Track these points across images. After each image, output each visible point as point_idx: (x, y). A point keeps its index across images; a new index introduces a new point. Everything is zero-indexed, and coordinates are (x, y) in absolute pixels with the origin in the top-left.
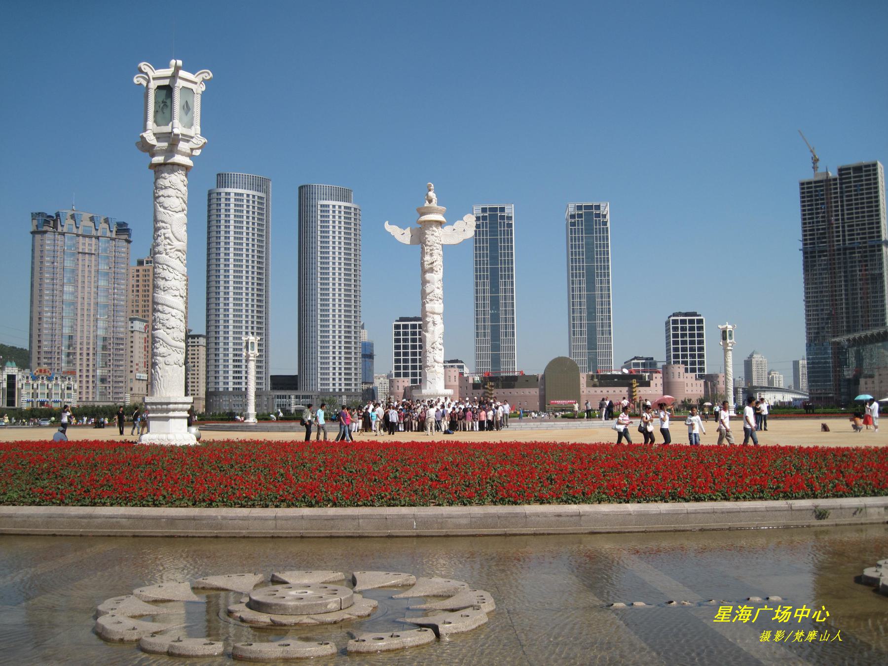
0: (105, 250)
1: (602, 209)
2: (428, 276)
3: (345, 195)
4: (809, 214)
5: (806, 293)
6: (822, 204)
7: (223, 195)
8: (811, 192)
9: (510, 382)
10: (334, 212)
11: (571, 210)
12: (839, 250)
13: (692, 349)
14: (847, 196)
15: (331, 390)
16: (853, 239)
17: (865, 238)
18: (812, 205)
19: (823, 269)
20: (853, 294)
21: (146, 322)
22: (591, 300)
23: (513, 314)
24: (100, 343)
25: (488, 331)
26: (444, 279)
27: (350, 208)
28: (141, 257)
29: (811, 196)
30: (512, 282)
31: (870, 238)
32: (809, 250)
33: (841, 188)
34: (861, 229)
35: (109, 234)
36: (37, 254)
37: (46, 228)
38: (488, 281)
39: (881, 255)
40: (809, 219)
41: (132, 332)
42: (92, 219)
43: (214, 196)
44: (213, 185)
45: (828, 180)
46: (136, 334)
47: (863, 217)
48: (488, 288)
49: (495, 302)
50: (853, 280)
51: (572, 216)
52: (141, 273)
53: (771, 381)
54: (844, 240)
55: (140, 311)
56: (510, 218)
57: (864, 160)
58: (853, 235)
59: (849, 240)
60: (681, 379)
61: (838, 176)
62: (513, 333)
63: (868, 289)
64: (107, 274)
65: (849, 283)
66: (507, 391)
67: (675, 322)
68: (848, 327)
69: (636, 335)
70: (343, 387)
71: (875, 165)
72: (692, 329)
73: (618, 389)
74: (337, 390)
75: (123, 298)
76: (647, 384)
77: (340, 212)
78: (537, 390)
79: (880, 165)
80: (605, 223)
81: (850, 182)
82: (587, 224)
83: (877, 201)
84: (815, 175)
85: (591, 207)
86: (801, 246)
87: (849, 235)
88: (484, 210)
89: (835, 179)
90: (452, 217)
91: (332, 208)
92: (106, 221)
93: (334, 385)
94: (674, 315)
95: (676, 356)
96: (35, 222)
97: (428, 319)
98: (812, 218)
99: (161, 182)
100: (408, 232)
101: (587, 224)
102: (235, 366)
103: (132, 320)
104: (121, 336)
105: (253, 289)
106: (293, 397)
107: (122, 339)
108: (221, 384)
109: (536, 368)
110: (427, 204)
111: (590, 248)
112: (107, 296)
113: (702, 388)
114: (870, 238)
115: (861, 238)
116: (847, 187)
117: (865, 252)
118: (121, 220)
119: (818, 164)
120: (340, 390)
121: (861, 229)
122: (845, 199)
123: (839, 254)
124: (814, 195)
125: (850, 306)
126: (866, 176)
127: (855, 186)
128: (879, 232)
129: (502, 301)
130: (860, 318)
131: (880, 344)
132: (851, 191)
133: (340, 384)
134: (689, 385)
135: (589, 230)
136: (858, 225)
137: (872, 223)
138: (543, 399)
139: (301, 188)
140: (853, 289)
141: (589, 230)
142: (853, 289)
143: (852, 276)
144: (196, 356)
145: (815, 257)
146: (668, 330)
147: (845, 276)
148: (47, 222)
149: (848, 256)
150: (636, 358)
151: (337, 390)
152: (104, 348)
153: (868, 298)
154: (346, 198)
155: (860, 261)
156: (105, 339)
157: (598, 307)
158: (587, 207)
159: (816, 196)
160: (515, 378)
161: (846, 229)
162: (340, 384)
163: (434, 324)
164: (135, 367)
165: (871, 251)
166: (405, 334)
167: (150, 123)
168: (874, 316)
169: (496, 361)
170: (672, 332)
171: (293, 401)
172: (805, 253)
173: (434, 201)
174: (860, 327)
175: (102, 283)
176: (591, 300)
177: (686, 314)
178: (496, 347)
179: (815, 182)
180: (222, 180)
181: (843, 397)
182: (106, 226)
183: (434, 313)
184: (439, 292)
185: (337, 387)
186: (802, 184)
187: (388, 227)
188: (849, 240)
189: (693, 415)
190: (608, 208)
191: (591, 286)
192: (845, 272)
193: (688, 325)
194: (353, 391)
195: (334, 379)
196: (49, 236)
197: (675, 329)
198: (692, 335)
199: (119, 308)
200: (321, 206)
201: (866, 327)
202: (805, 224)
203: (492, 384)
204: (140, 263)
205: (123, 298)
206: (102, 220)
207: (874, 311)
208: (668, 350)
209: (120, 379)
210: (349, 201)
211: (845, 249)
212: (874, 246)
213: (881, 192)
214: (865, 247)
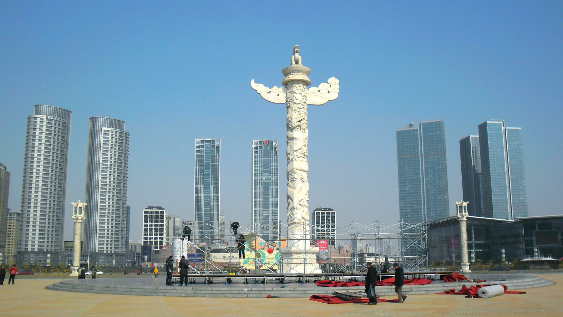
7: (39, 119)
67: (318, 214)
74: (109, 252)
94: (317, 210)
102: (40, 234)
108: (30, 246)
120: (111, 251)
124: (405, 139)
151: (109, 252)
162: (111, 248)
166: (152, 217)
170: (316, 220)
173: (300, 62)
185: (109, 250)
186: (398, 132)
187: (253, 85)
197: (318, 218)
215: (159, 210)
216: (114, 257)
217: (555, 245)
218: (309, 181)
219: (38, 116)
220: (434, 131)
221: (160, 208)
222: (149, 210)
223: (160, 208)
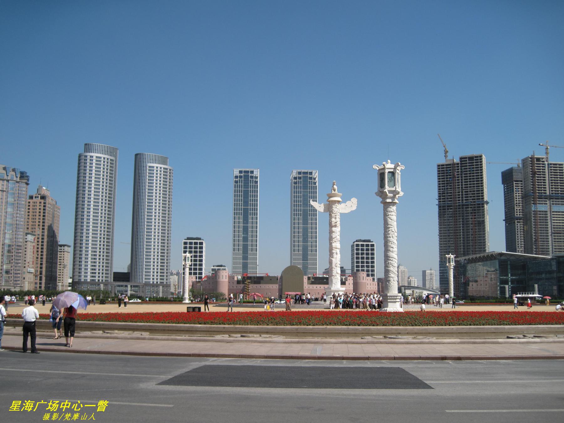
0: (12, 189)
1: (313, 174)
2: (334, 229)
3: (163, 161)
4: (442, 184)
5: (440, 231)
6: (450, 178)
7: (88, 157)
8: (444, 171)
9: (259, 280)
10: (157, 171)
11: (295, 174)
12: (459, 206)
13: (367, 263)
14: (465, 174)
15: (151, 283)
16: (468, 200)
17: (474, 199)
18: (444, 178)
19: (450, 217)
20: (467, 232)
21: (35, 235)
23: (257, 237)
24: (6, 248)
25: (241, 247)
26: (341, 231)
27: (167, 169)
28: (31, 194)
29: (444, 173)
30: (257, 218)
31: (477, 199)
32: (442, 205)
33: (461, 169)
34: (472, 194)
35: (15, 179)
38: (241, 216)
39: (484, 209)
40: (443, 186)
41: (26, 242)
42: (5, 169)
43: (83, 157)
44: (82, 151)
45: (454, 164)
46: (29, 244)
47: (474, 187)
48: (241, 220)
49: (246, 230)
50: (467, 224)
51: (295, 178)
52: (31, 204)
53: (409, 283)
54: (462, 200)
55: (30, 228)
56: (256, 178)
57: (475, 153)
58: (468, 197)
59: (466, 200)
60: (364, 281)
61: (459, 162)
62: (256, 249)
63: (476, 229)
64: (13, 204)
65: (465, 226)
66: (258, 285)
67: (357, 245)
68: (464, 251)
70: (159, 281)
71: (481, 156)
72: (367, 250)
74: (155, 283)
75: (22, 220)
77: (161, 171)
78: (277, 286)
79: (484, 157)
80: (315, 183)
81: (466, 166)
82: (304, 185)
83: (482, 178)
84: (446, 161)
85: (306, 173)
86: (437, 202)
87: (465, 197)
88: (241, 172)
89: (458, 164)
90: (345, 199)
91: (155, 168)
92: (14, 170)
93: (153, 279)
94: (357, 241)
97: (334, 251)
98: (444, 186)
99: (389, 209)
100: (322, 205)
103: (27, 234)
104: (20, 244)
105: (105, 217)
106: (129, 286)
107: (20, 246)
108: (83, 277)
109: (277, 272)
110: (333, 192)
112: (12, 218)
113: (377, 286)
114: (477, 199)
115: (472, 199)
116: (464, 169)
117: (475, 207)
118: (22, 170)
119: (448, 154)
120: (157, 282)
121: (472, 194)
122: (463, 175)
123: (459, 208)
124: (446, 173)
125: (466, 239)
126: (476, 162)
127: (469, 168)
128: (483, 196)
129: (250, 229)
130: (471, 247)
131: (480, 263)
132: (467, 171)
133: (157, 279)
134: (369, 284)
135: (305, 187)
136: (470, 191)
137: (479, 191)
138: (281, 291)
139: (136, 155)
140: (467, 229)
141: (305, 187)
142: (467, 229)
143: (467, 221)
144: (62, 258)
145: (445, 209)
146: (353, 250)
147: (463, 222)
149: (465, 209)
151: (155, 283)
152: (9, 251)
153: (476, 235)
154: (165, 163)
155: (471, 213)
156: (9, 246)
157: (310, 235)
158: (304, 173)
159: (447, 173)
160: (261, 278)
161: (464, 193)
162: (157, 279)
163: (337, 254)
164: (27, 264)
165: (478, 207)
167: (386, 186)
168: (479, 245)
169: (245, 266)
171: (129, 288)
172: (439, 207)
174: (471, 252)
175: (9, 210)
177: (364, 241)
178: (245, 258)
179: (446, 165)
180: (88, 148)
181: (462, 293)
182: (13, 173)
183: (336, 248)
184: (338, 237)
185: (155, 281)
186: (439, 166)
188: (466, 200)
190: (317, 174)
191: (305, 222)
192: (463, 219)
193: (365, 248)
194: (97, 281)
195: (153, 276)
197: (357, 250)
198: (367, 254)
199: (20, 226)
200: (149, 167)
201: (474, 252)
202: (439, 189)
203: (249, 281)
204: (31, 197)
205: (22, 220)
206: (11, 170)
207: (479, 243)
208: (353, 263)
209: (19, 272)
210: (166, 165)
211: (463, 205)
212: (479, 204)
214: (475, 205)
215: (198, 241)
216: (161, 287)
217: (518, 296)
218: (340, 254)
219: (89, 154)
220: (471, 166)
221: (199, 239)
222: (188, 241)
223: (199, 239)
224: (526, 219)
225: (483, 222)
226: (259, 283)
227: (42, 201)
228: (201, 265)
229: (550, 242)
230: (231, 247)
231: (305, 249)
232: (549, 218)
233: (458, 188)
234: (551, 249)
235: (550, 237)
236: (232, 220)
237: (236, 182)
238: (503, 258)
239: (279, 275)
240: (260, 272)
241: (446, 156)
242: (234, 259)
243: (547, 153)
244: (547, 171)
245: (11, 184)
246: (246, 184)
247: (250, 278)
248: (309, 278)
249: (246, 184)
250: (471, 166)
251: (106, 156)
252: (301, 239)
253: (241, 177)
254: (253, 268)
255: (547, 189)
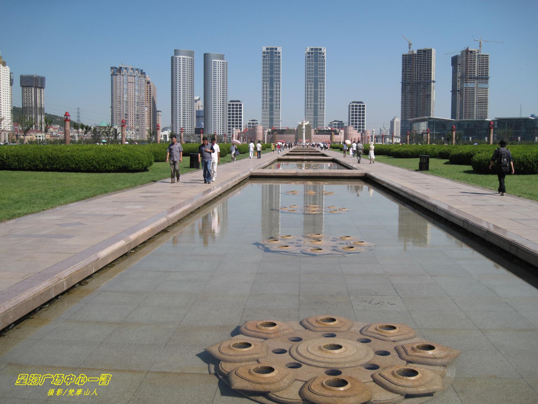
3: (222, 57)
9: (282, 132)
11: (308, 50)
22: (316, 93)
25: (268, 106)
36: (114, 83)
37: (117, 73)
38: (268, 83)
44: (173, 55)
45: (413, 55)
48: (268, 86)
49: (271, 93)
51: (309, 53)
56: (279, 53)
64: (138, 90)
66: (282, 135)
67: (353, 106)
69: (335, 110)
70: (222, 133)
71: (431, 50)
72: (360, 109)
73: (326, 136)
76: (338, 134)
80: (324, 57)
82: (315, 58)
88: (267, 49)
94: (353, 103)
95: (353, 121)
96: (112, 71)
101: (315, 58)
111: (316, 69)
119: (411, 46)
129: (275, 93)
135: (316, 60)
141: (316, 60)
148: (117, 71)
150: (335, 121)
154: (223, 59)
157: (319, 96)
169: (271, 120)
172: (402, 84)
176: (316, 93)
177: (358, 103)
178: (271, 114)
180: (176, 52)
186: (403, 55)
189: (131, 142)
190: (325, 50)
191: (316, 87)
196: (118, 76)
197: (353, 109)
198: (360, 112)
201: (417, 116)
208: (349, 118)
211: (418, 83)
213: (433, 61)
220: (425, 56)
221: (239, 101)
223: (239, 101)
224: (461, 91)
225: (430, 95)
226: (282, 134)
227: (149, 85)
228: (241, 120)
229: (475, 109)
230: (261, 106)
231: (316, 107)
232: (475, 92)
233: (416, 71)
234: (475, 113)
235: (475, 105)
236: (261, 86)
237: (264, 57)
238: (431, 120)
239: (296, 129)
240: (282, 126)
241: (410, 48)
242: (263, 114)
243: (480, 46)
244: (476, 60)
245: (136, 79)
246: (271, 58)
247: (276, 130)
248: (315, 131)
249: (271, 58)
250: (425, 56)
251: (188, 57)
252: (313, 100)
253: (267, 53)
254: (277, 121)
255: (476, 73)
